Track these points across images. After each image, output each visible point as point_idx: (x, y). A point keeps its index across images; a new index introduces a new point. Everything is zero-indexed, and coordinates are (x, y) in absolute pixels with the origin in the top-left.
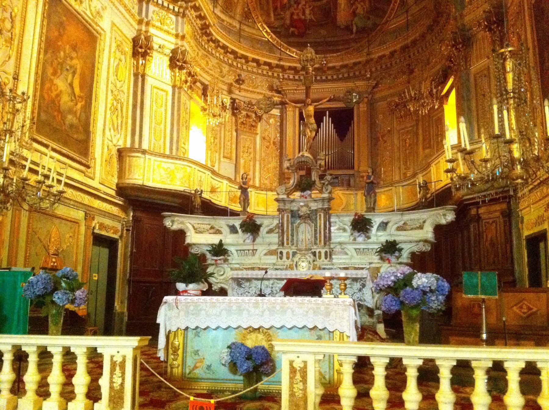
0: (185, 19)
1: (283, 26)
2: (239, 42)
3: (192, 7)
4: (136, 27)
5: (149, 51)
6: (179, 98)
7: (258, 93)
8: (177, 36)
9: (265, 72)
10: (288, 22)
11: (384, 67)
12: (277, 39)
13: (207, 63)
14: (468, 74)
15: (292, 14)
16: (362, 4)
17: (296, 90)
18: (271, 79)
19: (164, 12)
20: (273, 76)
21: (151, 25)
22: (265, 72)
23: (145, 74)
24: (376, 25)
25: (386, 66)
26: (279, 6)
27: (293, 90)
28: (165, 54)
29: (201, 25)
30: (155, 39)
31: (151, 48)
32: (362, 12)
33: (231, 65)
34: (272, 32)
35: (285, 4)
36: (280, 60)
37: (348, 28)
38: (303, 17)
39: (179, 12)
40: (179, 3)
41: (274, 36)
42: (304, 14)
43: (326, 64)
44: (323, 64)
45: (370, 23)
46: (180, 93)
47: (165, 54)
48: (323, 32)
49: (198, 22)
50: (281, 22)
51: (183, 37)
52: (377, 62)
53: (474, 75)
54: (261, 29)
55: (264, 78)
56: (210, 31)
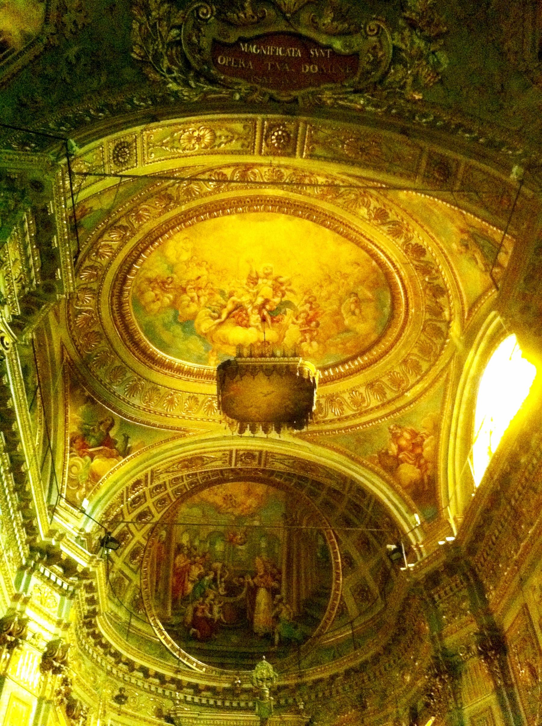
0: (73, 601)
1: (183, 623)
2: (127, 640)
3: (86, 586)
4: (9, 604)
5: (20, 641)
6: (45, 718)
7: (140, 719)
8: (59, 623)
9: (153, 688)
10: (189, 619)
11: (320, 695)
12: (172, 641)
13: (80, 665)
14: (460, 716)
15: (196, 610)
16: (288, 606)
17: (196, 719)
18: (161, 699)
19: (48, 588)
20: (164, 696)
21: (29, 604)
22: (153, 688)
23: (7, 674)
24: (306, 637)
25: (324, 694)
26: (180, 598)
27: (192, 718)
28: (38, 648)
29: (89, 611)
30: (29, 624)
31: (23, 638)
32: (287, 618)
33: (109, 673)
34: (166, 630)
35: (188, 596)
36: (178, 671)
37: (268, 637)
38: (210, 615)
39: (67, 591)
40: (71, 578)
41: (169, 637)
42: (211, 610)
43: (240, 684)
44: (236, 685)
45: (297, 634)
46: (47, 710)
47: (38, 648)
48: (234, 639)
49: (87, 608)
50: (179, 619)
51: (67, 626)
52: (311, 688)
53: (471, 719)
54: (152, 624)
55: (152, 696)
56: (95, 622)
